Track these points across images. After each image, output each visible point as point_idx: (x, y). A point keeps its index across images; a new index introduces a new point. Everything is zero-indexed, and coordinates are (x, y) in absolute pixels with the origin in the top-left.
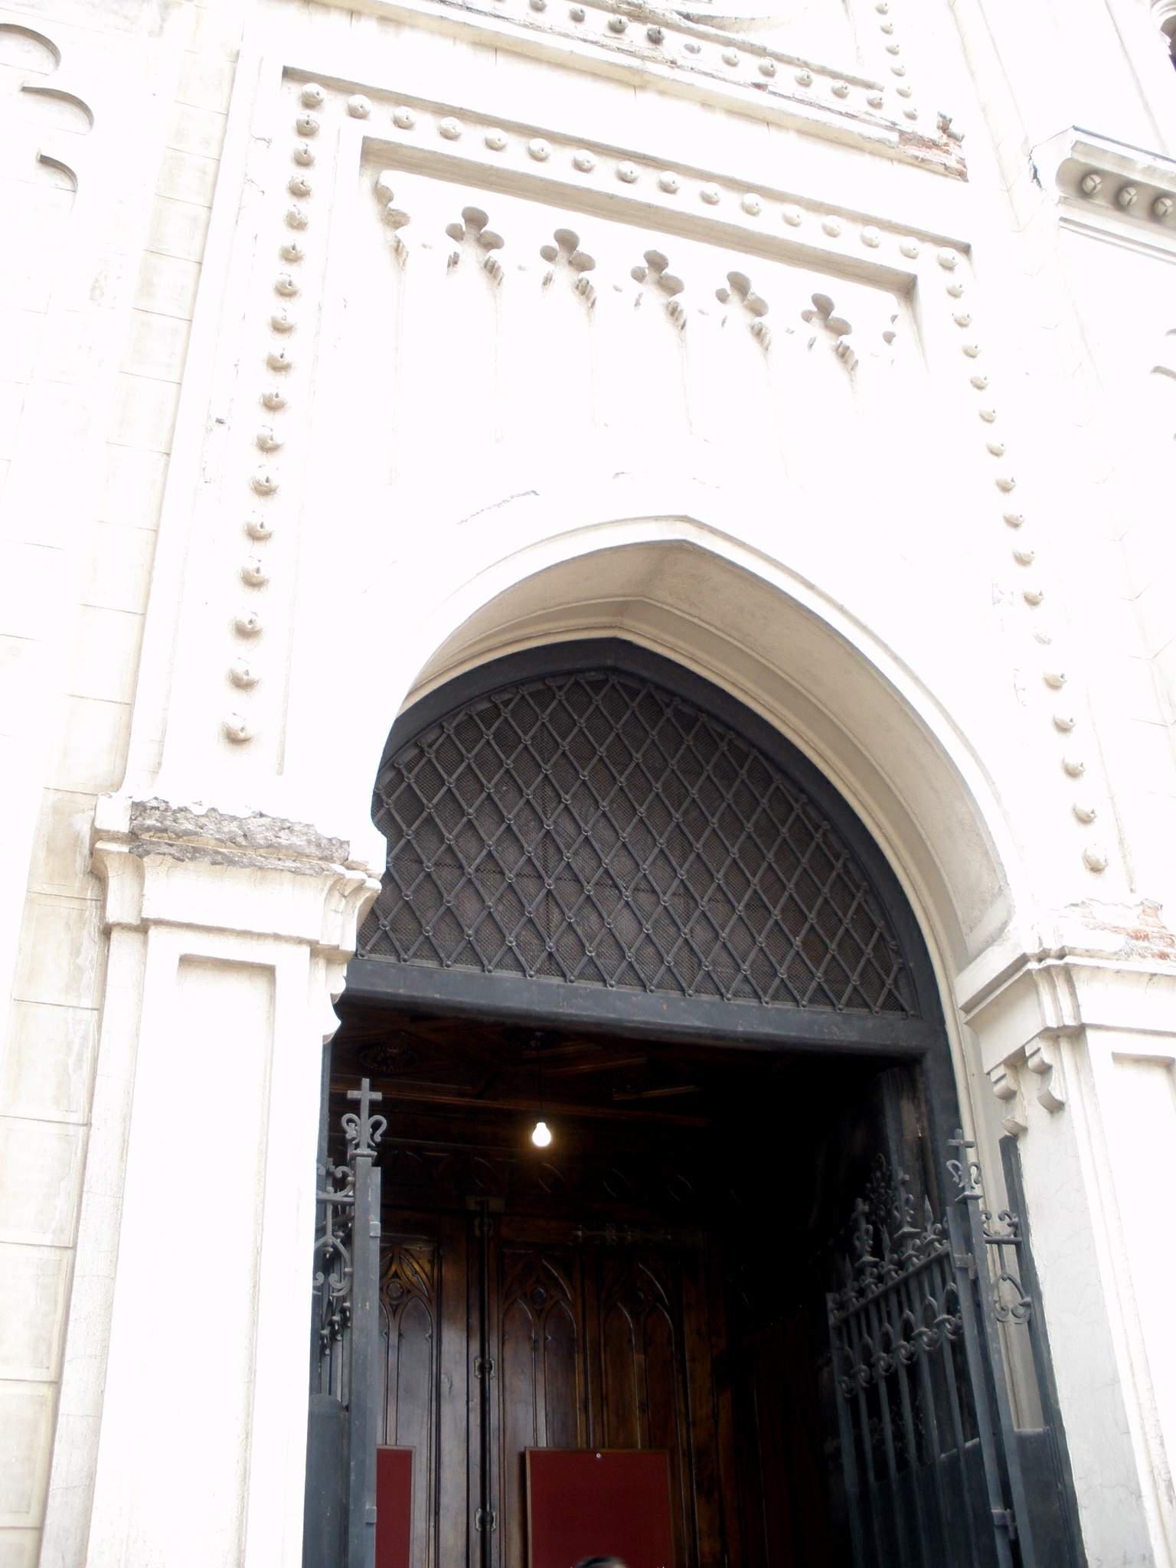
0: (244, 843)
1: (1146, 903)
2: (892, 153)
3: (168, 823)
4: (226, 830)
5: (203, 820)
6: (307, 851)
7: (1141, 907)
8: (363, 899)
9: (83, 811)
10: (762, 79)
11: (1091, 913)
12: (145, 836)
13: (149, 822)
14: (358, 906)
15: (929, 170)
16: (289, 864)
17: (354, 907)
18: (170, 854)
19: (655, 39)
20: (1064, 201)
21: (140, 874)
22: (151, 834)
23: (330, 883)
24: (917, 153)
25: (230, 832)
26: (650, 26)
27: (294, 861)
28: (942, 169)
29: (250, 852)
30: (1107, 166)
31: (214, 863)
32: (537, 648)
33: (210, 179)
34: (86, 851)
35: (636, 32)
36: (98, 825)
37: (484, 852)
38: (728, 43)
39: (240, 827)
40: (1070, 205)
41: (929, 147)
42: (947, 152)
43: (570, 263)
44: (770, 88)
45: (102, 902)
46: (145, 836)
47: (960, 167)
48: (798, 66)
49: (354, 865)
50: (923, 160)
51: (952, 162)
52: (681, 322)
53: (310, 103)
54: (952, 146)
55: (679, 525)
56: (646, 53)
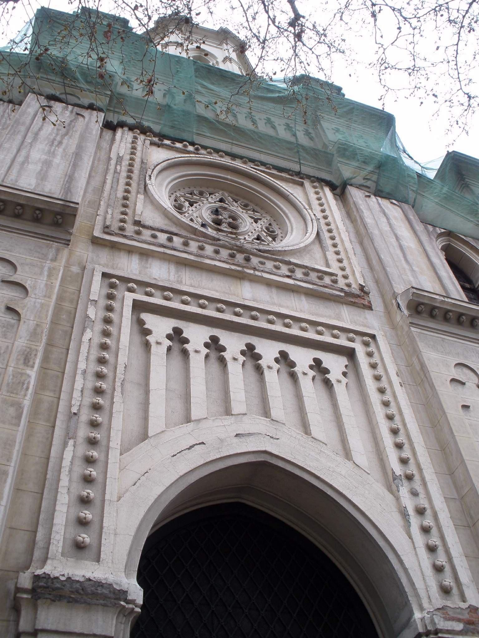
0: (82, 593)
1: (471, 607)
2: (342, 300)
3: (49, 584)
4: (75, 587)
5: (65, 583)
6: (109, 596)
7: (469, 609)
8: (133, 617)
9: (12, 579)
10: (289, 274)
11: (447, 612)
12: (39, 590)
13: (41, 584)
14: (131, 620)
15: (356, 306)
16: (102, 602)
17: (129, 621)
18: (50, 598)
19: (248, 259)
20: (410, 316)
21: (35, 608)
22: (42, 589)
23: (118, 610)
24: (352, 300)
25: (76, 588)
26: (245, 255)
27: (104, 600)
28: (362, 306)
29: (85, 597)
30: (426, 301)
31: (69, 602)
32: (207, 507)
33: (72, 316)
34: (12, 598)
35: (240, 257)
36: (19, 586)
37: (185, 594)
38: (276, 260)
39: (81, 586)
40: (413, 317)
41: (357, 298)
42: (364, 299)
43: (216, 349)
44: (293, 277)
45: (17, 622)
46: (39, 590)
47: (369, 304)
48: (304, 268)
49: (129, 602)
50: (355, 303)
51: (366, 303)
52: (261, 372)
53: (113, 286)
54: (366, 297)
55: (263, 455)
56: (244, 265)
